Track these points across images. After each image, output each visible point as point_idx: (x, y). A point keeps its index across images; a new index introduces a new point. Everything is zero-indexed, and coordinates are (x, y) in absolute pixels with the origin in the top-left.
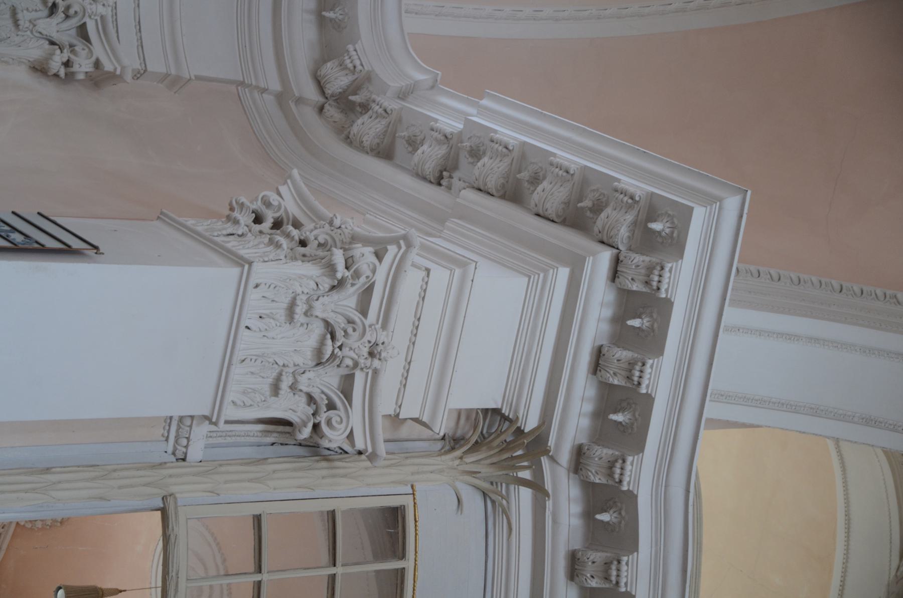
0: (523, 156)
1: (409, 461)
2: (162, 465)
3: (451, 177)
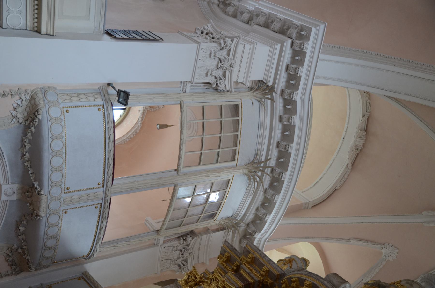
0: (269, 16)
1: (240, 93)
2: (180, 93)
3: (251, 22)
